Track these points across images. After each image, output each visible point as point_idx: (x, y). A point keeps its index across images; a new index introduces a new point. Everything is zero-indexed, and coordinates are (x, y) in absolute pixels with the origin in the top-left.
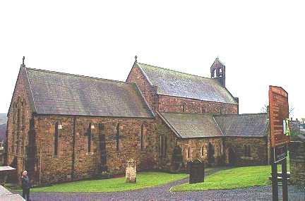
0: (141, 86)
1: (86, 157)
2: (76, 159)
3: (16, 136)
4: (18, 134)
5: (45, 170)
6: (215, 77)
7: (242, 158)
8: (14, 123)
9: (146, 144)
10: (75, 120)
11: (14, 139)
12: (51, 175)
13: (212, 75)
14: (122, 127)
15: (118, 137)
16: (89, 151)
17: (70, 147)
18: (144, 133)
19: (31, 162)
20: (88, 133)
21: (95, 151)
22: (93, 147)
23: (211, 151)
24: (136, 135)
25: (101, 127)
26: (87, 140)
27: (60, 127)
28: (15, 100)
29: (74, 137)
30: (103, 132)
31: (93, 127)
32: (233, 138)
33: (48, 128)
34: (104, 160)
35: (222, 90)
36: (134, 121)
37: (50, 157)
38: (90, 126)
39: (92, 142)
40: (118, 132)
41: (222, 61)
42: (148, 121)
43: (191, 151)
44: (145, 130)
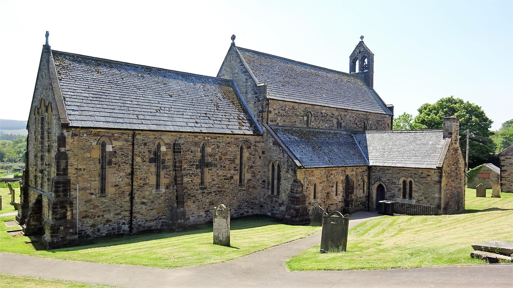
0: (245, 76)
2: (137, 200)
6: (357, 71)
9: (247, 176)
13: (352, 67)
14: (209, 150)
15: (203, 164)
18: (245, 159)
20: (156, 158)
21: (167, 188)
22: (164, 181)
24: (233, 161)
27: (109, 148)
28: (37, 103)
31: (163, 149)
37: (93, 196)
39: (162, 173)
40: (203, 156)
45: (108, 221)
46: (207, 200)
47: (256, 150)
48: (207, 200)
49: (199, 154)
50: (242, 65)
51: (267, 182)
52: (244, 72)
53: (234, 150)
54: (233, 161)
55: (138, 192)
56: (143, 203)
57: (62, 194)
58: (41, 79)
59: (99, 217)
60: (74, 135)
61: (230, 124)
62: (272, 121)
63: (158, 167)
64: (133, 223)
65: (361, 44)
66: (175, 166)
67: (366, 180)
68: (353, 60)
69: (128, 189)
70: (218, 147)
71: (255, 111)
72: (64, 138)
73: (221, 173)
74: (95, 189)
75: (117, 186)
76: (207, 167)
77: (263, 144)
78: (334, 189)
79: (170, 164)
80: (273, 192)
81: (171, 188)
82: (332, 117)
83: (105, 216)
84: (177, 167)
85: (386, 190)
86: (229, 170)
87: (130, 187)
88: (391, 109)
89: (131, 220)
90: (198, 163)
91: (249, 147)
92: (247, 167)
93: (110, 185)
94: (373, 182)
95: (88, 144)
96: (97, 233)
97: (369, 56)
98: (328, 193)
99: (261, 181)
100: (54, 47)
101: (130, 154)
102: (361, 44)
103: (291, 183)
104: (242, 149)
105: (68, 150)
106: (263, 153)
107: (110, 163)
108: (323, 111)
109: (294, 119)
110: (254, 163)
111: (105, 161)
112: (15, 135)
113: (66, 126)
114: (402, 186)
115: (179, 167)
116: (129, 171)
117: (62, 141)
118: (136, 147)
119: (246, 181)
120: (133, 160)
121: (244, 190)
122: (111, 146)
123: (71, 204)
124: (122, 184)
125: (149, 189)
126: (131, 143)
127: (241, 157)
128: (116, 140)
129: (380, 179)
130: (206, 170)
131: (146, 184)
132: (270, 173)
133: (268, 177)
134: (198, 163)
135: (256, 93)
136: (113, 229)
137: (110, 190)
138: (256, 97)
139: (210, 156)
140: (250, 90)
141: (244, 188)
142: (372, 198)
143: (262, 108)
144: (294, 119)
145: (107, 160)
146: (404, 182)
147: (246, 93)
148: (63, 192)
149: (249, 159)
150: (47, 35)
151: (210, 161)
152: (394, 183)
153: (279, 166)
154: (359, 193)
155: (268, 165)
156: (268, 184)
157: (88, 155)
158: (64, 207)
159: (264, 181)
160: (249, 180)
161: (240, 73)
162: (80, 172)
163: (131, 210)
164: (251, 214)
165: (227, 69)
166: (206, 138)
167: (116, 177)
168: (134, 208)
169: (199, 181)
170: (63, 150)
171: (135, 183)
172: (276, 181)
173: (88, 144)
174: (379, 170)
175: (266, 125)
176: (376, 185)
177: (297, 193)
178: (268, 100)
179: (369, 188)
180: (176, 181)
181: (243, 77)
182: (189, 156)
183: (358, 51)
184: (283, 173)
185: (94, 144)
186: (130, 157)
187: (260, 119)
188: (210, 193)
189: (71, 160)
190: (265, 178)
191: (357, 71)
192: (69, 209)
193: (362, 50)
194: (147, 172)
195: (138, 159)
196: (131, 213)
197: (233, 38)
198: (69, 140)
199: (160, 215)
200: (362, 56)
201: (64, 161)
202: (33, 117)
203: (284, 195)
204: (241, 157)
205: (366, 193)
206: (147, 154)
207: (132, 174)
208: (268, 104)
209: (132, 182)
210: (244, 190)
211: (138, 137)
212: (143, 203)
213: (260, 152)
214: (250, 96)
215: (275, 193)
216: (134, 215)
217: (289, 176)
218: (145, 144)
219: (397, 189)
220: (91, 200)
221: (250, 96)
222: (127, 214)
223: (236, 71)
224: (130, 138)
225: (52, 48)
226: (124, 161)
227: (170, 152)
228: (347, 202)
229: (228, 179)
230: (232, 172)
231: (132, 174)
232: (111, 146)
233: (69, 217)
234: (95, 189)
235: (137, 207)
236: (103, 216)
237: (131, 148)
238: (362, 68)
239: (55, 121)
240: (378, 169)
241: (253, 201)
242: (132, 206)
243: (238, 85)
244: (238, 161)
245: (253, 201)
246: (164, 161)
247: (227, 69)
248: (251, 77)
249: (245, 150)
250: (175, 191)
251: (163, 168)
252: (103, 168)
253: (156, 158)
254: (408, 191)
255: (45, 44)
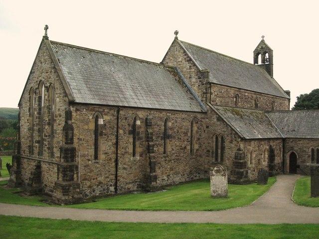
0: (187, 64)
1: (131, 165)
2: (120, 166)
3: (36, 134)
4: (40, 131)
5: (85, 179)
6: (260, 62)
7: (308, 164)
8: (31, 115)
9: (196, 147)
10: (118, 112)
11: (32, 136)
12: (152, 134)
13: (256, 61)
14: (170, 124)
15: (166, 136)
16: (134, 155)
17: (113, 149)
18: (194, 132)
19: (68, 171)
20: (134, 131)
21: (141, 156)
22: (139, 150)
23: (272, 157)
24: (186, 134)
25: (147, 123)
26: (131, 140)
27: (101, 122)
28: (33, 85)
29: (117, 136)
30: (150, 131)
31: (138, 123)
32: (296, 139)
33: (87, 124)
34: (152, 166)
35: (269, 77)
36: (184, 116)
37: (90, 162)
38: (135, 121)
39: (137, 143)
40: (165, 130)
41: (269, 43)
42: (199, 116)
43: (254, 156)
44: (195, 128)
45: (100, 183)
46: (169, 167)
47: (202, 125)
48: (169, 167)
49: (163, 128)
50: (185, 55)
51: (211, 151)
52: (188, 61)
53: (187, 124)
54: (186, 134)
55: (121, 159)
56: (124, 168)
57: (70, 159)
58: (40, 64)
59: (94, 179)
60: (77, 110)
61: (175, 100)
62: (213, 101)
63: (134, 139)
64: (118, 185)
65: (263, 41)
66: (148, 138)
67: (282, 150)
68: (256, 54)
69: (114, 156)
70: (176, 122)
71: (199, 92)
72: (71, 112)
73: (178, 144)
74: (91, 156)
75: (106, 153)
76: (168, 139)
77: (207, 120)
78: (263, 156)
79: (143, 135)
80: (216, 159)
81: (144, 156)
82: (252, 99)
83: (98, 179)
84: (149, 138)
85: (298, 157)
86: (184, 141)
87: (115, 155)
88: (288, 93)
89: (116, 183)
90: (162, 135)
91: (197, 123)
92: (196, 139)
93: (102, 152)
94: (287, 151)
95: (87, 117)
96: (93, 193)
97: (270, 51)
98: (259, 160)
99: (205, 151)
100: (51, 38)
101: (116, 126)
102: (263, 41)
103: (234, 152)
104: (192, 124)
105: (73, 123)
106: (207, 127)
107: (101, 134)
108: (246, 94)
109: (227, 100)
110: (200, 136)
111: (98, 132)
112: (295, 106)
113: (72, 103)
114: (310, 154)
115: (151, 138)
116: (114, 141)
117: (69, 115)
118: (120, 120)
119: (195, 151)
120: (117, 132)
121: (193, 158)
122: (102, 120)
123: (77, 167)
124: (110, 152)
125: (129, 156)
126: (116, 118)
127: (192, 131)
128: (105, 115)
129: (292, 148)
130: (168, 141)
131: (126, 152)
132: (214, 143)
133: (213, 147)
134: (162, 135)
135: (199, 78)
136: (104, 190)
137: (102, 157)
138: (200, 81)
139: (171, 129)
140: (193, 75)
141: (194, 157)
142: (287, 164)
143: (206, 90)
144: (227, 100)
145: (99, 131)
146: (313, 150)
147: (190, 78)
148: (71, 158)
149: (197, 132)
150: (46, 28)
151: (170, 133)
152: (305, 151)
153: (222, 138)
154: (278, 160)
155: (212, 138)
156: (213, 153)
157: (86, 127)
158: (72, 171)
159: (208, 151)
160: (197, 150)
161: (184, 61)
162: (81, 142)
163: (116, 174)
164: (197, 178)
165: (171, 58)
166: (168, 114)
167: (106, 146)
168: (118, 172)
169: (163, 150)
170: (70, 122)
171: (119, 152)
172: (219, 151)
173: (87, 117)
174: (292, 142)
175: (209, 104)
176: (289, 153)
177: (241, 160)
178: (210, 83)
179: (283, 156)
180: (149, 149)
181: (188, 65)
182: (156, 129)
183: (260, 47)
184: (227, 144)
185: (91, 117)
186: (115, 129)
187: (204, 99)
188: (171, 160)
189: (76, 132)
190: (209, 148)
191: (260, 62)
192: (75, 172)
193: (264, 46)
194: (127, 141)
195: (121, 131)
196: (116, 177)
197: (176, 33)
198: (74, 114)
199: (136, 178)
200: (263, 50)
201: (71, 132)
202: (27, 96)
203: (227, 161)
204: (192, 131)
205: (282, 160)
206: (127, 127)
207: (117, 144)
208: (210, 87)
209: (117, 151)
210: (193, 158)
211: (121, 112)
212: (124, 168)
213: (205, 126)
214: (194, 80)
215: (219, 160)
216: (118, 178)
217: (233, 146)
218: (126, 119)
219: (307, 156)
220: (88, 166)
221: (194, 80)
222: (113, 177)
223: (180, 60)
224: (115, 113)
225: (50, 39)
226: (111, 132)
227: (143, 126)
228: (271, 166)
229: (182, 149)
230: (186, 143)
231: (117, 144)
232: (102, 120)
233: (75, 179)
234: (91, 156)
235: (120, 172)
236: (97, 178)
237: (116, 121)
238: (264, 60)
239: (58, 99)
240: (291, 140)
241: (200, 167)
242: (117, 171)
243: (182, 71)
244: (189, 134)
245: (200, 167)
246: (138, 133)
247: (171, 58)
248: (195, 65)
249: (194, 125)
250: (148, 158)
251: (138, 139)
252: (96, 140)
253: (134, 131)
254: (219, 155)
255: (44, 35)
